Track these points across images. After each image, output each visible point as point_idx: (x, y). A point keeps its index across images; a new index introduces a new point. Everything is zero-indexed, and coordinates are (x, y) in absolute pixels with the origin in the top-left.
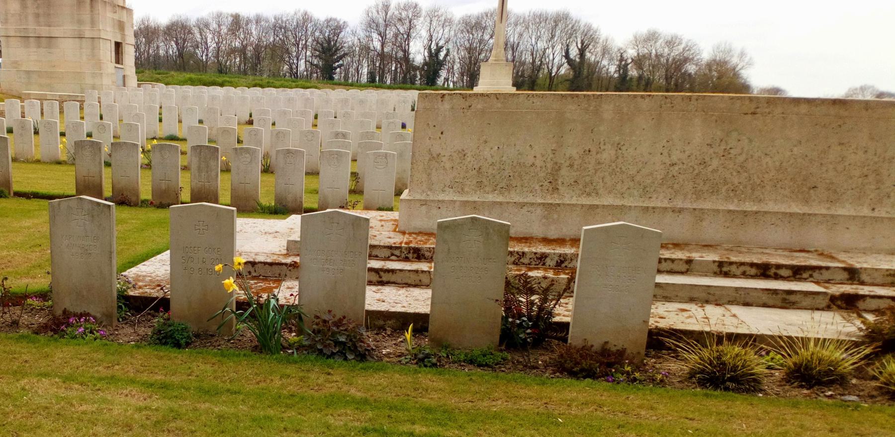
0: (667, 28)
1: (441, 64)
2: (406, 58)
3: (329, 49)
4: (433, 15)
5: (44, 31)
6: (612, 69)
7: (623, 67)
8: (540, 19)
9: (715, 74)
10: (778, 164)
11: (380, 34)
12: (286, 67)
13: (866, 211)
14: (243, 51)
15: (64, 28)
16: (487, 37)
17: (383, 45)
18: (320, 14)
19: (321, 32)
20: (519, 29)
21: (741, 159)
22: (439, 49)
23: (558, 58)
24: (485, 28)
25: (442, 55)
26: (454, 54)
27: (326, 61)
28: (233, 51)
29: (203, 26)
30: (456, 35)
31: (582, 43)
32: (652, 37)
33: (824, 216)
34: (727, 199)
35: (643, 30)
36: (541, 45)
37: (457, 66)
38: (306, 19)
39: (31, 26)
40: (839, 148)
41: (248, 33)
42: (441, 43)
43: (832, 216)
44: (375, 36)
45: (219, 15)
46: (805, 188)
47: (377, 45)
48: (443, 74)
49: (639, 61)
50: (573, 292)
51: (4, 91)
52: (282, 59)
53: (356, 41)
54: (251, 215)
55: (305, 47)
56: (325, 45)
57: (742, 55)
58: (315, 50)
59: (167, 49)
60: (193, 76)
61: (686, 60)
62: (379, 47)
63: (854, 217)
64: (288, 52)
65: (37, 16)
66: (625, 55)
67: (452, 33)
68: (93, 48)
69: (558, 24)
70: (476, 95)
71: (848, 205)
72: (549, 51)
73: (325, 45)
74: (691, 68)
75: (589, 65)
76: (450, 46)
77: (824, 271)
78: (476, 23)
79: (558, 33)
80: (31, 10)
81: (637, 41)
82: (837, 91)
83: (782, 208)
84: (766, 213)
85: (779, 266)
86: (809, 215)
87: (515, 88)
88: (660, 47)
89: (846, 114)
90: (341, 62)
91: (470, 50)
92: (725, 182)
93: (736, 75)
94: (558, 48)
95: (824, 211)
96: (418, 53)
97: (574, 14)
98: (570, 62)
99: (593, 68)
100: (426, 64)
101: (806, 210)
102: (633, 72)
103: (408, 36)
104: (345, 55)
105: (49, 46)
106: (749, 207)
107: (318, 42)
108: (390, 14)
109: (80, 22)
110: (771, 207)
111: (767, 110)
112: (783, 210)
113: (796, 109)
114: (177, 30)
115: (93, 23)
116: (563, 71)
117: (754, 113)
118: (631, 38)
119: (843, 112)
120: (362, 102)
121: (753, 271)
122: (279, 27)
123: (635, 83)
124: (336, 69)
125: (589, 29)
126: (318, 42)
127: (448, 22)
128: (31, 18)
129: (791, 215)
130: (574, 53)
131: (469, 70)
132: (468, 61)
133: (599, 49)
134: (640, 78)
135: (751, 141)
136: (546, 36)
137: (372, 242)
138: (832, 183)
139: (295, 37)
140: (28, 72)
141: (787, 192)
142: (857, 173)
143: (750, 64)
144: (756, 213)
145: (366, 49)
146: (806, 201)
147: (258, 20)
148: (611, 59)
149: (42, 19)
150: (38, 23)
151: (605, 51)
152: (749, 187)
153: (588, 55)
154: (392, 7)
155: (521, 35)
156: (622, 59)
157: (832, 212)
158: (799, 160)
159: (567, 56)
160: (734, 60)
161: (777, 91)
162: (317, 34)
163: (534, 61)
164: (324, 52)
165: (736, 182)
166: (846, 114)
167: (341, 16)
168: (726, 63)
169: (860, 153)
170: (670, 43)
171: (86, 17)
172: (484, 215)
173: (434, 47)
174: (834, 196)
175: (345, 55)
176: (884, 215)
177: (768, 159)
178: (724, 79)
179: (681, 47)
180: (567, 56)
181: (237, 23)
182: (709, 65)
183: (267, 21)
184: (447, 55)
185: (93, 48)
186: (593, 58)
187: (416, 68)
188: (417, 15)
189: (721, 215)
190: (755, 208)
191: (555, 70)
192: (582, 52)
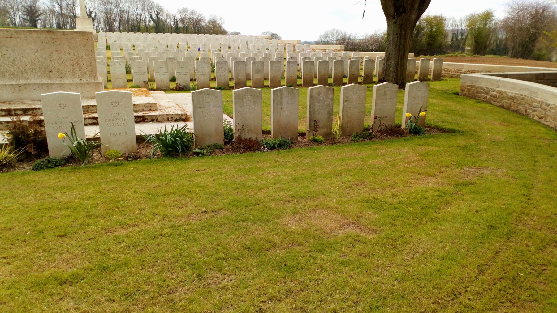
0: (191, 8)
3: (32, 11)
6: (172, 23)
7: (176, 23)
9: (212, 26)
10: (30, 61)
11: (58, 4)
12: (9, 20)
13: (78, 81)
17: (61, 9)
19: (26, 2)
20: (128, 4)
21: (12, 59)
22: (91, 12)
23: (148, 19)
24: (111, 3)
26: (99, 15)
27: (31, 17)
30: (98, 6)
32: (185, 10)
33: (58, 84)
34: (10, 79)
35: (181, 8)
37: (102, 21)
40: (57, 53)
42: (91, 9)
43: (61, 84)
44: (56, 5)
46: (48, 72)
47: (57, 9)
49: (182, 20)
52: (5, 16)
53: (46, 7)
55: (18, 10)
56: (29, 9)
58: (24, 11)
61: (200, 20)
62: (59, 11)
63: (72, 84)
64: (8, 12)
67: (96, 5)
70: (76, 32)
71: (69, 79)
72: (143, 15)
73: (29, 9)
74: (202, 24)
76: (97, 11)
77: (38, 110)
79: (146, 7)
83: (38, 81)
84: (29, 84)
85: (16, 110)
86: (51, 84)
88: (188, 15)
89: (55, 37)
90: (40, 18)
91: (106, 13)
92: (7, 71)
93: (220, 27)
94: (147, 13)
95: (58, 82)
98: (153, 20)
99: (164, 22)
101: (50, 82)
102: (181, 25)
103: (74, 5)
104: (41, 14)
106: (21, 82)
107: (24, 7)
110: (33, 81)
111: (17, 36)
112: (38, 82)
113: (31, 35)
117: (11, 38)
119: (53, 37)
120: (217, 40)
121: (4, 113)
123: (182, 30)
124: (37, 21)
125: (159, 6)
126: (24, 7)
129: (42, 84)
130: (154, 16)
131: (108, 22)
132: (106, 19)
133: (165, 15)
134: (183, 27)
135: (13, 51)
136: (140, 8)
137: (134, 103)
138: (59, 69)
139: (11, 5)
141: (39, 74)
142: (69, 64)
144: (25, 84)
145: (53, 12)
146: (49, 78)
148: (170, 19)
151: (167, 15)
152: (20, 73)
153: (161, 17)
155: (129, 7)
156: (175, 19)
157: (62, 82)
158: (40, 59)
159: (151, 17)
160: (218, 21)
162: (23, 3)
163: (137, 19)
164: (29, 12)
165: (12, 70)
166: (55, 37)
168: (215, 22)
169: (67, 55)
170: (193, 13)
174: (62, 76)
175: (41, 14)
176: (85, 82)
177: (24, 59)
180: (151, 17)
182: (209, 22)
184: (95, 15)
189: (8, 87)
190: (25, 83)
191: (147, 23)
192: (157, 15)
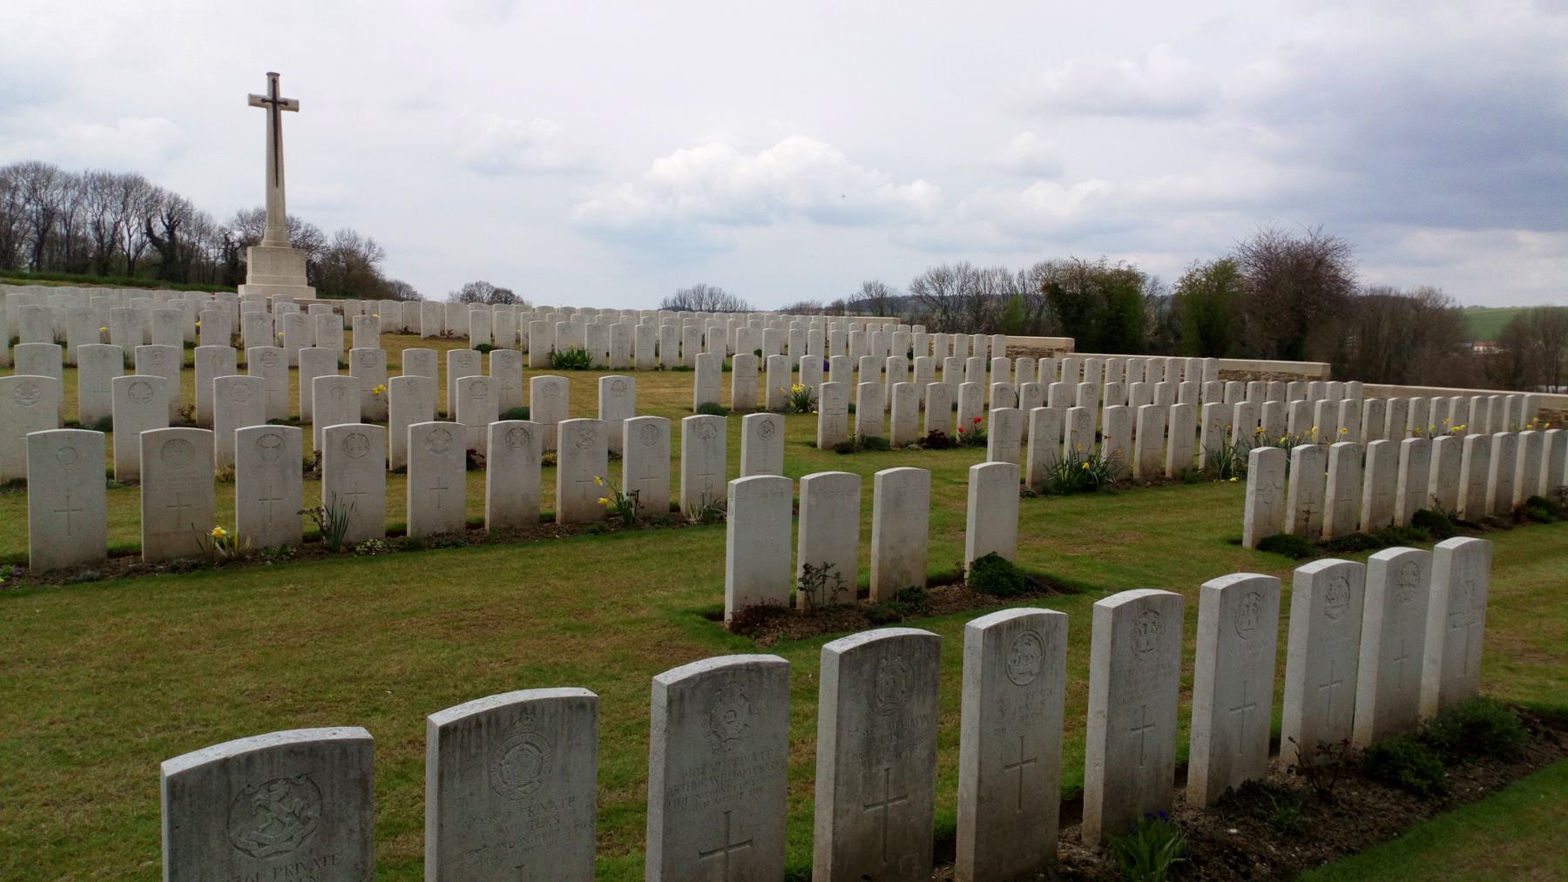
8: (103, 184)
16: (20, 201)
24: (16, 188)
31: (170, 219)
36: (109, 218)
50: (319, 476)
54: (1558, 712)
57: (370, 245)
75: (183, 247)
87: (313, 291)
94: (134, 222)
98: (155, 241)
99: (191, 251)
116: (220, 261)
125: (177, 200)
130: (159, 229)
143: (381, 256)
151: (203, 230)
153: (177, 233)
155: (75, 202)
159: (150, 232)
160: (363, 250)
172: (884, 521)
178: (354, 272)
179: (302, 230)
186: (186, 237)
192: (171, 229)
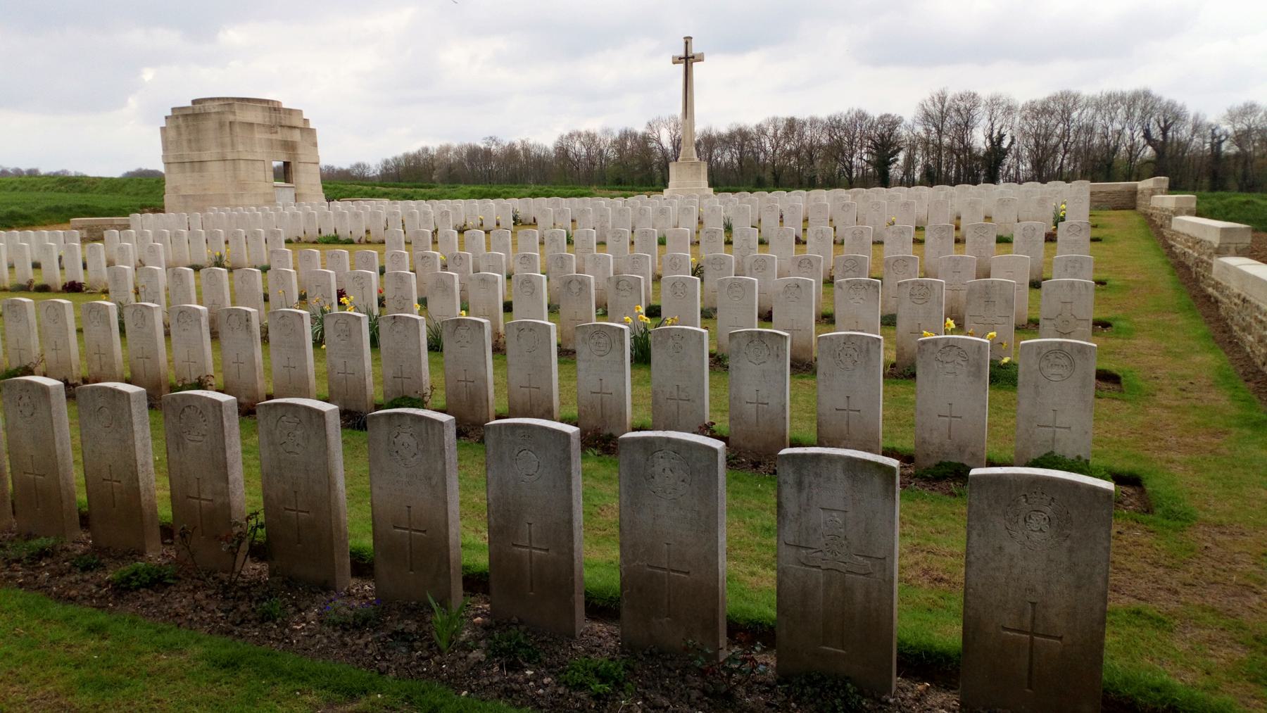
1: (1005, 153)
2: (968, 148)
4: (994, 103)
5: (195, 156)
14: (797, 153)
15: (211, 153)
18: (875, 112)
22: (1001, 137)
25: (1005, 144)
28: (790, 153)
29: (762, 131)
31: (1165, 122)
38: (862, 116)
39: (190, 154)
41: (801, 136)
45: (775, 120)
47: (934, 136)
48: (1009, 160)
49: (1241, 138)
51: (1166, 233)
59: (726, 157)
60: (477, 188)
65: (190, 141)
66: (1217, 132)
68: (235, 169)
69: (1141, 103)
78: (1044, 109)
80: (184, 137)
81: (1232, 117)
82: (346, 166)
96: (979, 140)
97: (1155, 92)
100: (988, 153)
105: (201, 170)
108: (946, 104)
109: (223, 145)
114: (740, 138)
115: (233, 145)
118: (1226, 113)
122: (833, 125)
127: (1009, 110)
128: (185, 144)
130: (1156, 133)
134: (1237, 156)
140: (184, 196)
147: (814, 122)
149: (193, 145)
150: (190, 148)
154: (949, 98)
161: (65, 171)
167: (895, 110)
171: (227, 140)
173: (995, 135)
180: (1147, 135)
181: (791, 125)
183: (822, 122)
184: (1012, 143)
185: (235, 169)
187: (977, 158)
188: (975, 105)
192: (1164, 131)
